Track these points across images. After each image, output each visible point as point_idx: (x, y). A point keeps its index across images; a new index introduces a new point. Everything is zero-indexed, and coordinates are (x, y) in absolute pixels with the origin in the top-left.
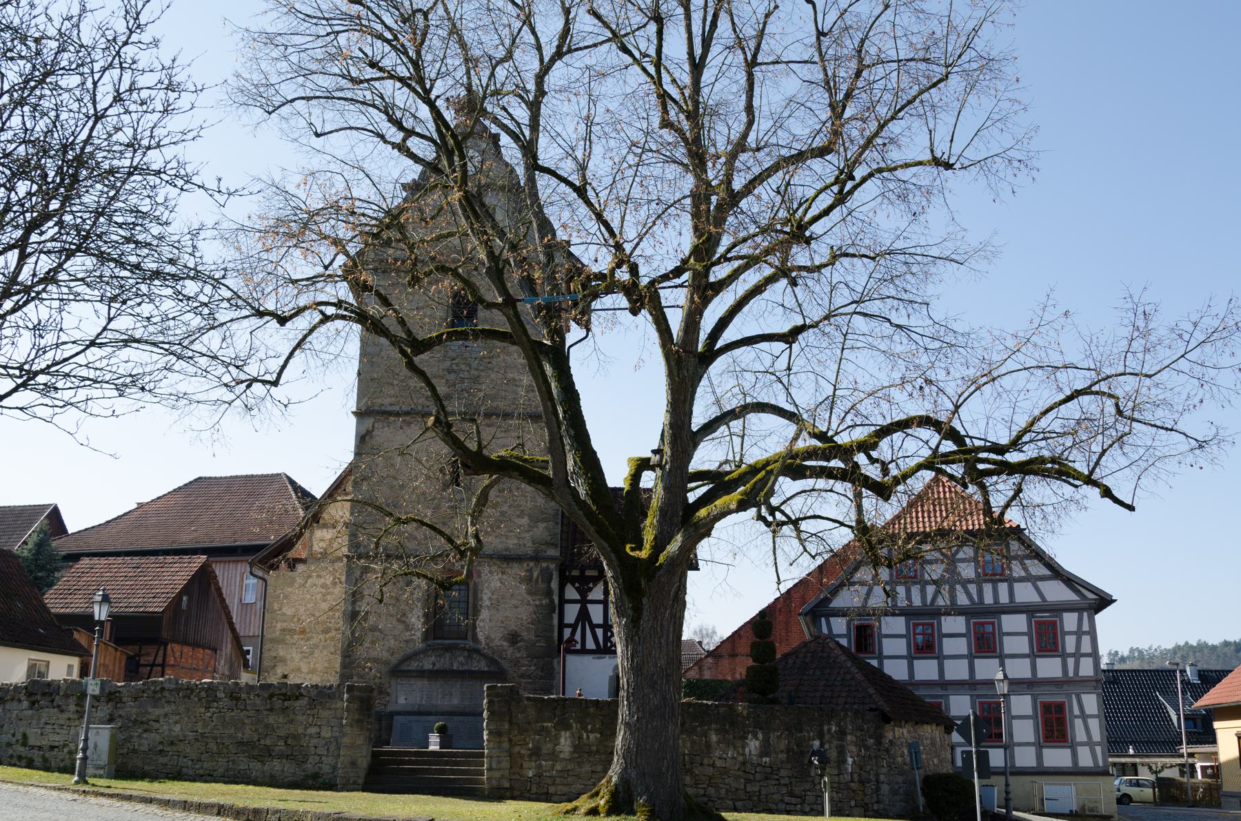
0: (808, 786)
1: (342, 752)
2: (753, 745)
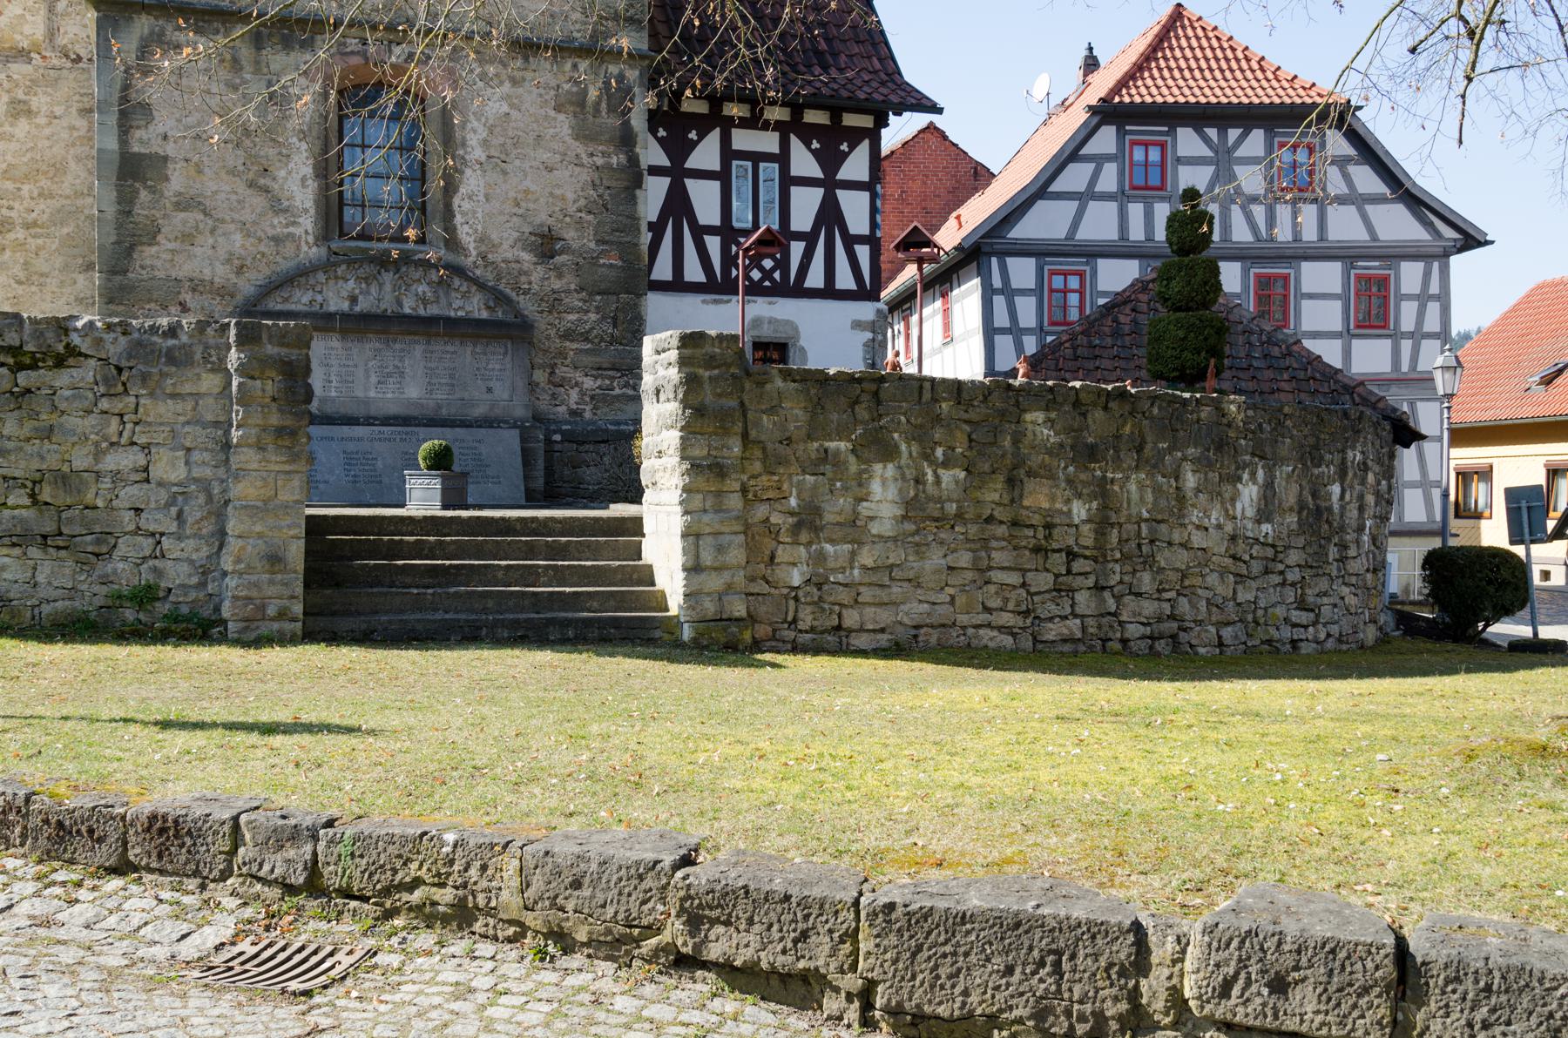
1: (232, 526)
2: (1249, 494)
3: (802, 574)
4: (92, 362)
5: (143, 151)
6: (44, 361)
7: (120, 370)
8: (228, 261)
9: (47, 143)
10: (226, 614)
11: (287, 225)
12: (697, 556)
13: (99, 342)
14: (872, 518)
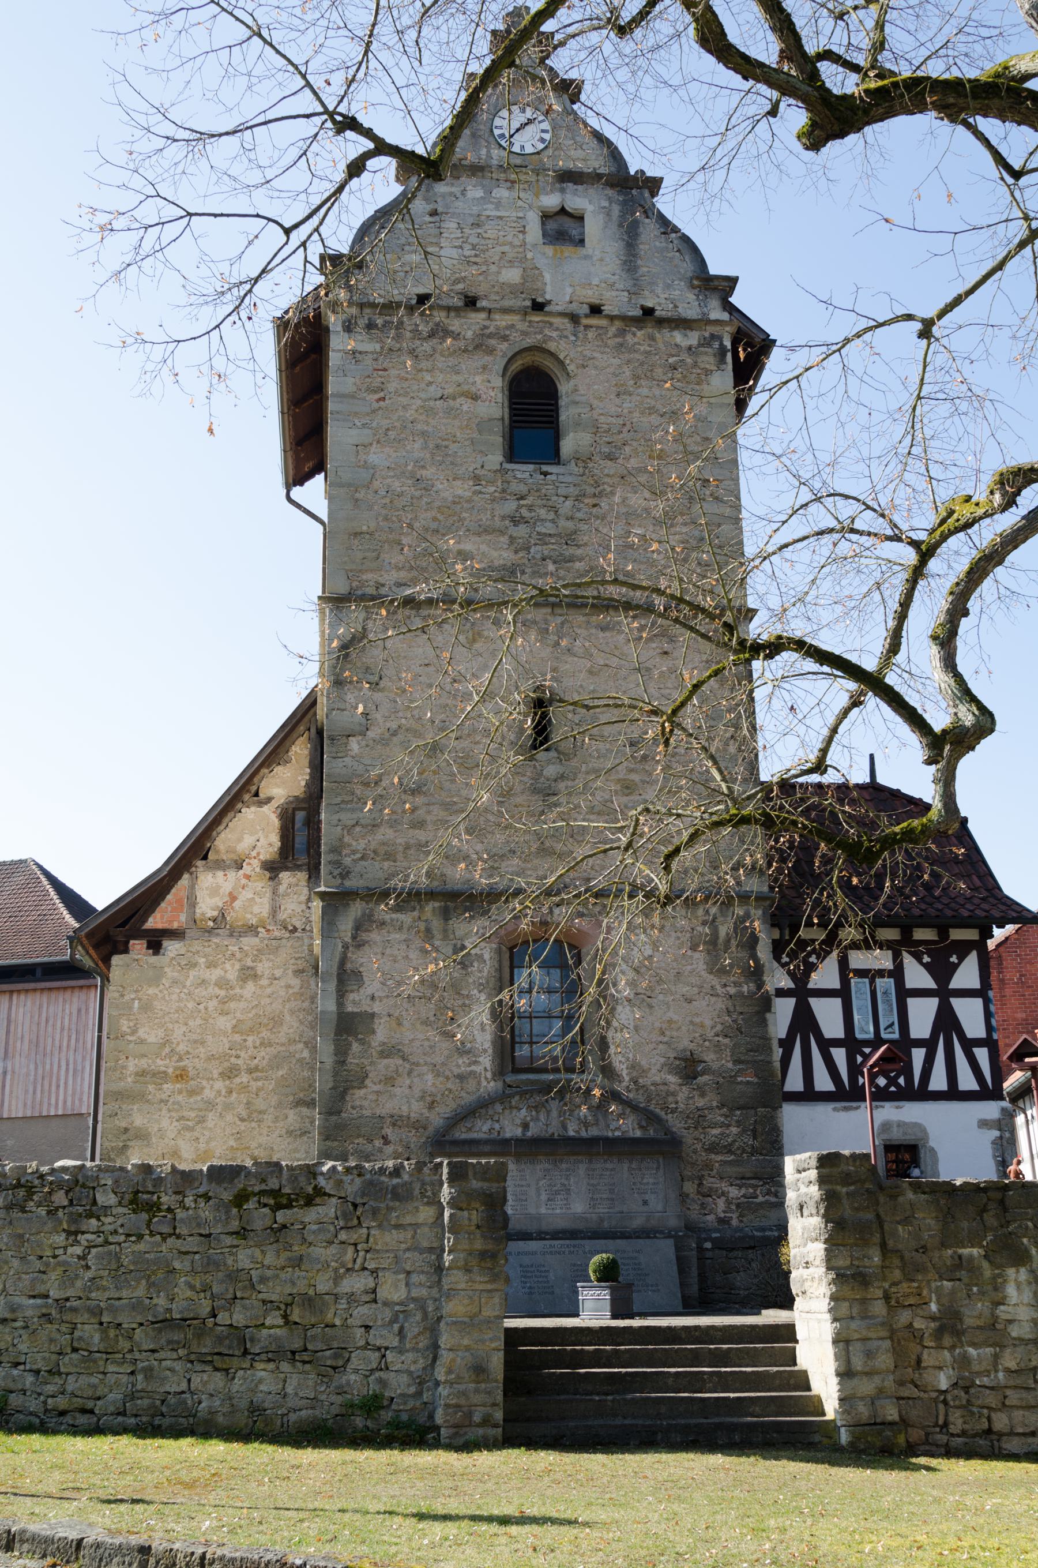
1: (444, 1341)
3: (949, 1378)
4: (334, 1200)
5: (356, 1010)
6: (297, 1200)
7: (355, 1206)
8: (422, 1098)
9: (268, 1001)
10: (439, 1419)
11: (470, 1065)
12: (848, 1361)
13: (339, 1183)
14: (1010, 1322)
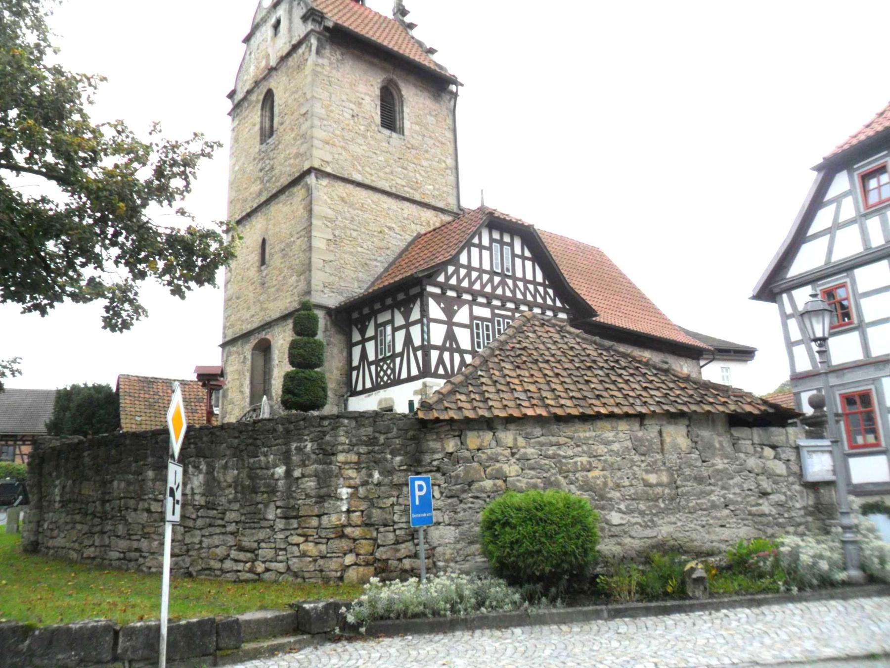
0: (261, 535)
